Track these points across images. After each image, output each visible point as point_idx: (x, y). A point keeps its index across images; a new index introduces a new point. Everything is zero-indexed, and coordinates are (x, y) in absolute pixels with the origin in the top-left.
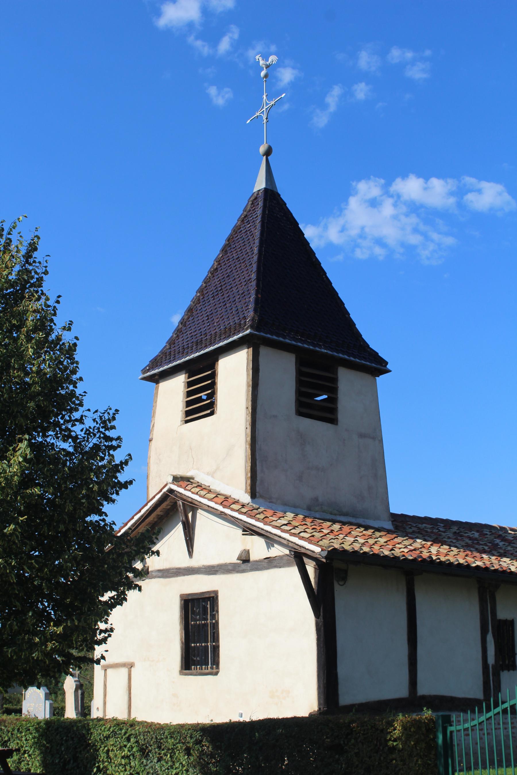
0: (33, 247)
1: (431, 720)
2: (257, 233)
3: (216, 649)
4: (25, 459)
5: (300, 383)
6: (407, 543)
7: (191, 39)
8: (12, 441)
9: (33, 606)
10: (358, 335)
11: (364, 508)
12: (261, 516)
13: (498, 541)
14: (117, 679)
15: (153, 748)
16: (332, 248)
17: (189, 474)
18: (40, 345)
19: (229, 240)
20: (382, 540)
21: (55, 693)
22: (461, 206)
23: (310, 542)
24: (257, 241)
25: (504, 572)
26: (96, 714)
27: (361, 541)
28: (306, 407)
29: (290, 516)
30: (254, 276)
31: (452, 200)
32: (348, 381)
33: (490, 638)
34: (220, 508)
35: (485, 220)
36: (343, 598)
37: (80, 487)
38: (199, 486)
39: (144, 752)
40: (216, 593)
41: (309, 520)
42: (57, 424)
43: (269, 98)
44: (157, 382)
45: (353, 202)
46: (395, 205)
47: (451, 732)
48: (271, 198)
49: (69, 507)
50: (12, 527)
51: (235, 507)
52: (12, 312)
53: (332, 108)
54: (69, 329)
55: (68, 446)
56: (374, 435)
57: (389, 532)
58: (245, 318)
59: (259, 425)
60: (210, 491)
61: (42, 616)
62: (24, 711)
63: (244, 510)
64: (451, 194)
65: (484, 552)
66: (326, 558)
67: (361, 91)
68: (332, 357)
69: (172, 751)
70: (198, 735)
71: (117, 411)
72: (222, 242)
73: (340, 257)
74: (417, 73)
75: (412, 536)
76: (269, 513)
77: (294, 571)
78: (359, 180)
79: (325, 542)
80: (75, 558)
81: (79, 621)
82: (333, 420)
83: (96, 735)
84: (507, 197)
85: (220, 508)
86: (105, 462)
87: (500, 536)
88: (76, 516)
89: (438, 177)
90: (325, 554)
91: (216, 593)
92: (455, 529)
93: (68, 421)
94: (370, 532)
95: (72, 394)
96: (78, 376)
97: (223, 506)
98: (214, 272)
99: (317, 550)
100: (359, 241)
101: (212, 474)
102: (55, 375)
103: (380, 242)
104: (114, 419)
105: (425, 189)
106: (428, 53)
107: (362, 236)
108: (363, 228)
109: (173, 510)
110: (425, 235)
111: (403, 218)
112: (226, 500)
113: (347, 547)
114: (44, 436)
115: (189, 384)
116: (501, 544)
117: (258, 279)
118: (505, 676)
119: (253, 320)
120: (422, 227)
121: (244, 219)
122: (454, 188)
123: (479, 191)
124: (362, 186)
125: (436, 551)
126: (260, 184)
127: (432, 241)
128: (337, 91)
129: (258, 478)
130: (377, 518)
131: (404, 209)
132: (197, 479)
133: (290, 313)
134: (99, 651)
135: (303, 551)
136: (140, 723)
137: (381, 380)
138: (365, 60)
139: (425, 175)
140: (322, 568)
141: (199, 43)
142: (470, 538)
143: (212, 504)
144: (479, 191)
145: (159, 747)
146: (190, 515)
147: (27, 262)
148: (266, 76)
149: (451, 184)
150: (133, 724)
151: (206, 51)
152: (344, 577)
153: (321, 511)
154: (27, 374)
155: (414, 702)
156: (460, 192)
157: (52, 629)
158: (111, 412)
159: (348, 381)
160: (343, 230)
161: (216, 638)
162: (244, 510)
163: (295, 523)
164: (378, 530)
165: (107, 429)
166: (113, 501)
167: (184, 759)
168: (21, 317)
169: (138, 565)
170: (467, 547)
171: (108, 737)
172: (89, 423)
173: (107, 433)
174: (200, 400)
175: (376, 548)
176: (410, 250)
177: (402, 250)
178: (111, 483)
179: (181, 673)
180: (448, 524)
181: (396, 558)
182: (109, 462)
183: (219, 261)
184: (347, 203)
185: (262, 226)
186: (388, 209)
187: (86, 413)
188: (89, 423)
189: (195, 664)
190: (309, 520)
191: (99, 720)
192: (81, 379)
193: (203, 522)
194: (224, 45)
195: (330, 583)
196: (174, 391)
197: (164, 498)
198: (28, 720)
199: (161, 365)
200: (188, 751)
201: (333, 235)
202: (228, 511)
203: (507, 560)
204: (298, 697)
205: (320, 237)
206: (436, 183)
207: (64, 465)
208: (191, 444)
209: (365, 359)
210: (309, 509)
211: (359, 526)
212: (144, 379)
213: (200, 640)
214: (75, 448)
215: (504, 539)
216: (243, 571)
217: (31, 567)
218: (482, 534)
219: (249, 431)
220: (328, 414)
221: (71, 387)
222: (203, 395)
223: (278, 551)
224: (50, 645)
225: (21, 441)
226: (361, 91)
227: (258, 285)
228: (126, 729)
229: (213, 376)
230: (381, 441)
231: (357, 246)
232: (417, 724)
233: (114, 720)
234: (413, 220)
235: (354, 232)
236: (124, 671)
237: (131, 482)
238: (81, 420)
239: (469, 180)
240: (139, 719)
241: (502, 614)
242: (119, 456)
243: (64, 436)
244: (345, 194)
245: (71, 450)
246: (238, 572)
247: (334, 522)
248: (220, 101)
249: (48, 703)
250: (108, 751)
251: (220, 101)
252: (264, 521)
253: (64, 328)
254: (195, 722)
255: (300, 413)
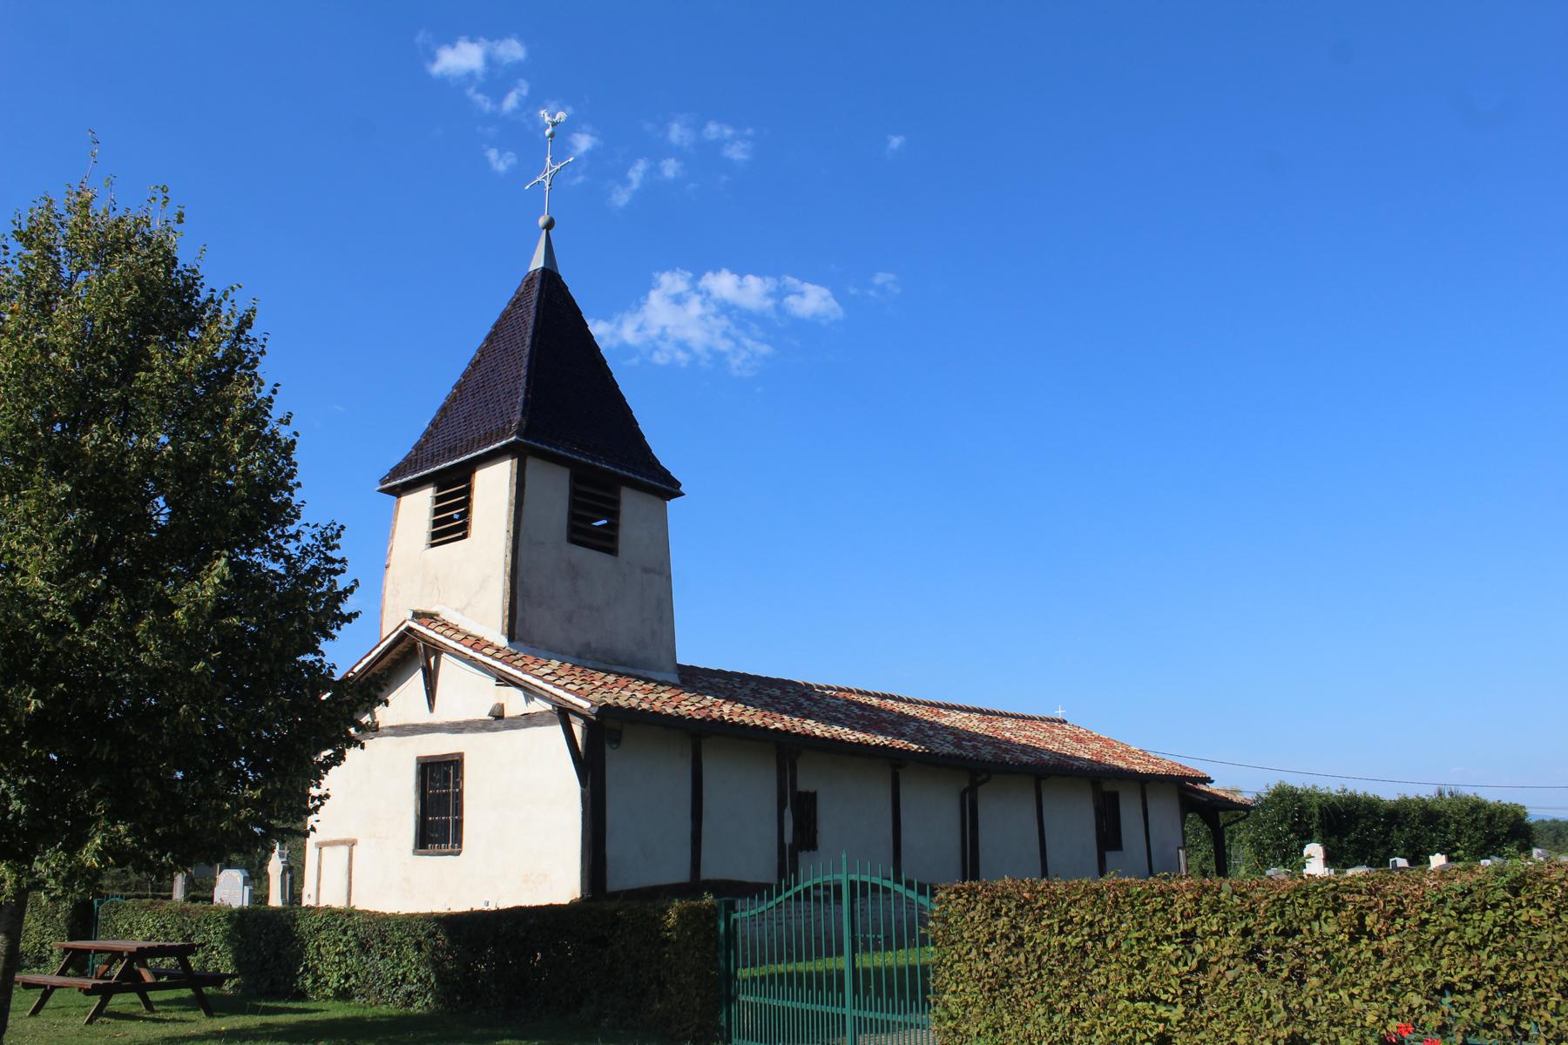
0: (246, 323)
1: (712, 906)
2: (531, 321)
3: (459, 824)
4: (223, 581)
5: (574, 504)
6: (694, 700)
7: (470, 91)
8: (208, 558)
9: (225, 765)
10: (646, 450)
11: (647, 655)
12: (520, 663)
13: (802, 700)
14: (335, 859)
15: (376, 942)
16: (626, 350)
17: (433, 610)
18: (249, 440)
19: (496, 326)
20: (665, 696)
21: (256, 877)
22: (779, 309)
23: (578, 696)
24: (530, 331)
25: (807, 736)
26: (306, 902)
27: (640, 696)
28: (580, 533)
29: (555, 663)
30: (524, 372)
31: (770, 303)
32: (631, 503)
33: (788, 813)
34: (470, 652)
35: (807, 328)
36: (617, 764)
37: (291, 619)
38: (445, 624)
39: (364, 947)
40: (461, 755)
41: (577, 671)
42: (266, 540)
43: (554, 161)
44: (399, 496)
45: (654, 297)
46: (703, 304)
47: (736, 921)
48: (550, 280)
49: (276, 644)
50: (202, 664)
51: (489, 651)
52: (214, 398)
53: (635, 186)
54: (288, 423)
55: (278, 567)
56: (661, 570)
57: (674, 686)
58: (510, 422)
59: (522, 552)
60: (458, 631)
61: (235, 777)
62: (216, 899)
63: (499, 655)
64: (769, 295)
65: (785, 712)
66: (596, 715)
67: (670, 168)
68: (615, 474)
69: (399, 946)
70: (431, 927)
71: (343, 527)
72: (487, 329)
73: (635, 361)
74: (737, 153)
75: (702, 692)
76: (530, 659)
77: (557, 730)
78: (663, 271)
79: (596, 696)
80: (281, 706)
81: (283, 783)
82: (612, 551)
83: (304, 926)
84: (833, 303)
85: (470, 652)
86: (324, 589)
87: (805, 695)
88: (285, 656)
89: (757, 274)
90: (595, 710)
91: (461, 755)
92: (753, 685)
93: (280, 537)
94: (651, 686)
95: (287, 503)
96: (295, 480)
97: (474, 651)
98: (475, 364)
99: (586, 705)
100: (659, 343)
101: (461, 611)
102: (266, 478)
103: (683, 345)
104: (338, 536)
105: (740, 287)
106: (750, 131)
107: (663, 336)
108: (664, 328)
109: (411, 653)
110: (738, 343)
111: (711, 318)
112: (478, 643)
113: (622, 703)
114: (249, 554)
115: (438, 500)
116: (806, 703)
117: (528, 376)
118: (803, 857)
119: (520, 424)
120: (733, 331)
121: (516, 303)
122: (773, 289)
123: (802, 294)
124: (666, 279)
125: (728, 710)
126: (538, 262)
127: (745, 348)
128: (641, 166)
129: (519, 617)
130: (661, 670)
131: (713, 309)
132: (442, 616)
133: (560, 418)
134: (311, 820)
135: (569, 706)
136: (360, 912)
137: (672, 504)
138: (677, 133)
139: (740, 271)
140: (590, 726)
141: (480, 97)
142: (770, 696)
143: (460, 647)
144: (802, 294)
145: (383, 942)
146: (432, 660)
147: (238, 338)
148: (552, 135)
149: (770, 284)
150: (350, 913)
151: (488, 106)
152: (617, 739)
153: (591, 658)
154: (230, 475)
155: (694, 887)
156: (780, 294)
157: (249, 793)
158: (336, 528)
159: (631, 503)
160: (640, 329)
161: (459, 810)
162: (499, 655)
163: (560, 673)
164: (662, 684)
165: (332, 548)
166: (333, 637)
167: (413, 955)
168: (228, 402)
169: (366, 719)
170: (765, 706)
171: (319, 930)
172: (306, 540)
173: (329, 553)
174: (451, 519)
175: (658, 704)
176: (718, 357)
177: (708, 357)
178: (330, 615)
179: (415, 853)
180: (745, 678)
181: (681, 717)
182: (330, 589)
183: (481, 351)
184: (647, 298)
185: (537, 313)
186: (695, 308)
187: (304, 528)
188: (306, 540)
189: (433, 843)
190: (577, 671)
191: (309, 908)
192: (299, 485)
193: (450, 670)
194: (511, 102)
195: (600, 747)
196: (419, 506)
197: (401, 638)
198: (219, 909)
199: (404, 475)
200: (418, 946)
201: (629, 333)
202: (479, 656)
203: (811, 722)
204: (561, 884)
205: (613, 335)
206: (753, 281)
207: (273, 590)
208: (439, 572)
209: (654, 478)
210: (579, 656)
211: (638, 678)
212: (382, 491)
213: (439, 812)
214: (288, 570)
215: (809, 698)
216: (496, 730)
217: (223, 716)
218: (785, 692)
219: (509, 559)
220: (606, 542)
221: (286, 495)
222: (455, 513)
223: (538, 706)
224: (243, 813)
225: (218, 557)
226: (670, 168)
227: (528, 383)
228: (342, 919)
229: (468, 491)
230: (669, 577)
231: (656, 348)
232: (696, 912)
233: (328, 908)
234: (724, 322)
235: (654, 332)
236: (344, 850)
237: (356, 615)
238: (296, 537)
239: (790, 281)
240: (359, 908)
241: (804, 785)
242: (342, 582)
243: (274, 554)
244: (647, 286)
245: (282, 571)
246: (489, 730)
247: (609, 673)
248: (501, 167)
249: (247, 889)
250: (319, 947)
251: (501, 167)
252: (522, 669)
253: (281, 421)
254: (429, 911)
255: (572, 540)
